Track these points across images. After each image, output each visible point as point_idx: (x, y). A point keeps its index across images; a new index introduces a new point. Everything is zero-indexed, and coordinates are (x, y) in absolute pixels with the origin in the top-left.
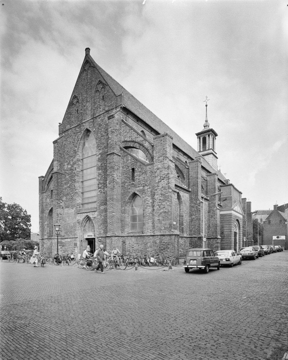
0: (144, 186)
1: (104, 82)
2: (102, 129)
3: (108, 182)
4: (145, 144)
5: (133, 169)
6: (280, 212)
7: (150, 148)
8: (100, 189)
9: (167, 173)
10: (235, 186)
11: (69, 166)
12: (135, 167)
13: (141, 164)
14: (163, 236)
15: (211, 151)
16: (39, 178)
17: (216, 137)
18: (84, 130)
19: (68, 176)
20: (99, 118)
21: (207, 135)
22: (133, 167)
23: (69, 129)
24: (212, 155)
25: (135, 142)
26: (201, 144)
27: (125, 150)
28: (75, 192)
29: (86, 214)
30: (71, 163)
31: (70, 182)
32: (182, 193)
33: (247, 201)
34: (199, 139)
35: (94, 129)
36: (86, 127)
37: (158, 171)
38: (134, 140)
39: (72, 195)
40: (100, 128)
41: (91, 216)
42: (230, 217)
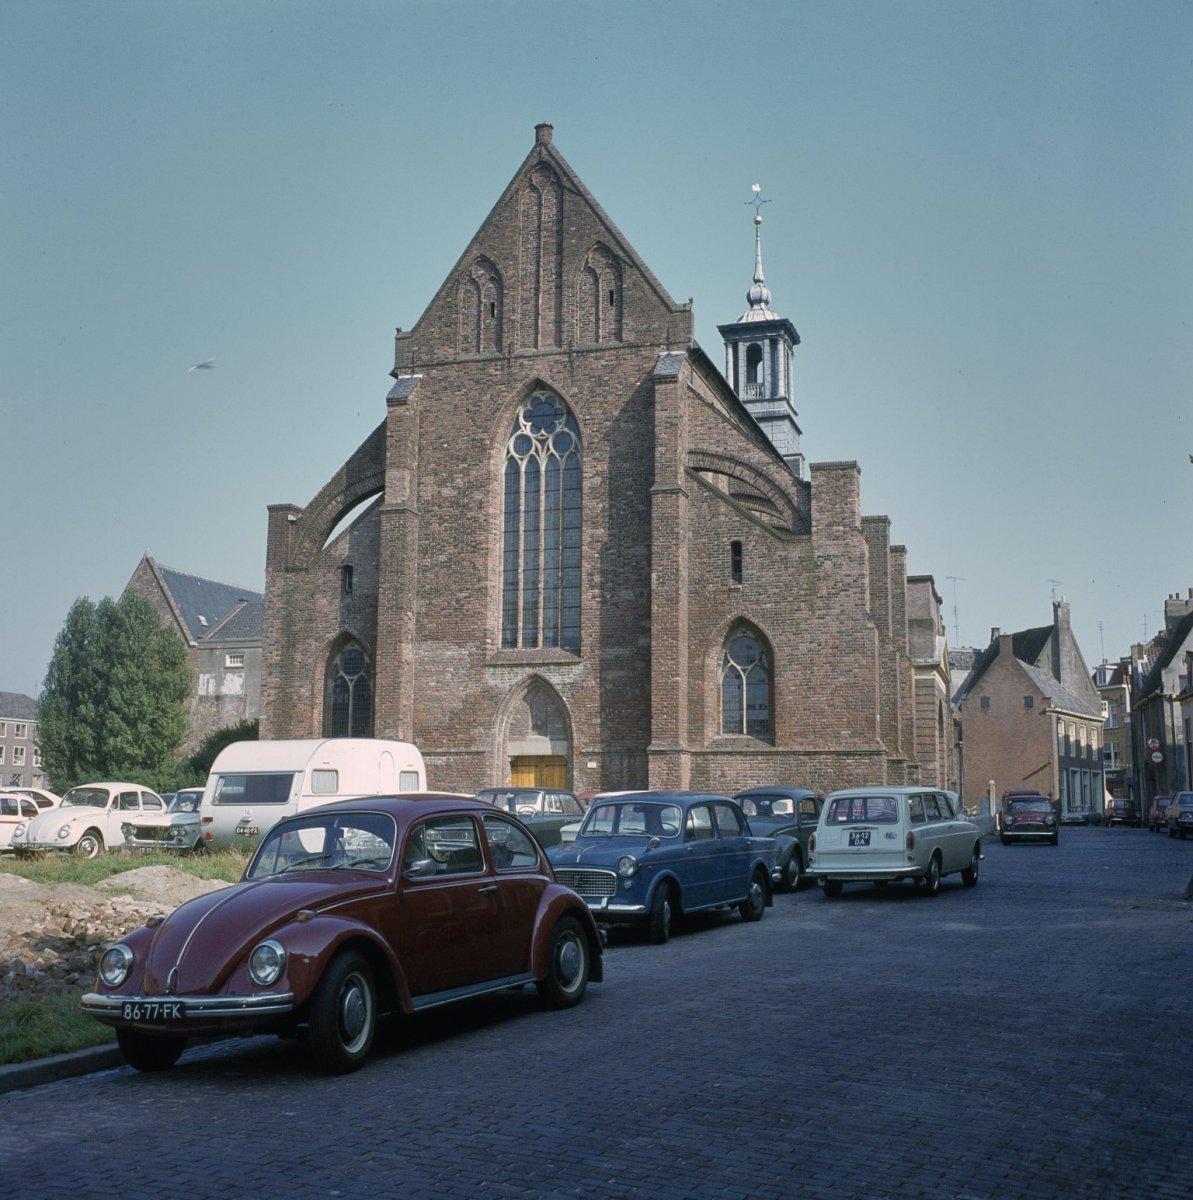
0: (777, 603)
1: (621, 253)
2: (610, 398)
3: (654, 576)
4: (777, 476)
5: (737, 547)
6: (1024, 664)
7: (792, 490)
9: (856, 572)
10: (936, 586)
12: (742, 539)
13: (767, 534)
14: (846, 755)
15: (782, 408)
16: (271, 509)
17: (795, 347)
20: (596, 359)
21: (767, 342)
22: (736, 539)
23: (453, 363)
24: (787, 423)
25: (739, 463)
26: (742, 363)
28: (477, 586)
29: (529, 671)
30: (459, 482)
34: (730, 351)
35: (576, 390)
36: (534, 374)
37: (828, 565)
38: (735, 454)
40: (599, 390)
41: (555, 679)
42: (930, 691)
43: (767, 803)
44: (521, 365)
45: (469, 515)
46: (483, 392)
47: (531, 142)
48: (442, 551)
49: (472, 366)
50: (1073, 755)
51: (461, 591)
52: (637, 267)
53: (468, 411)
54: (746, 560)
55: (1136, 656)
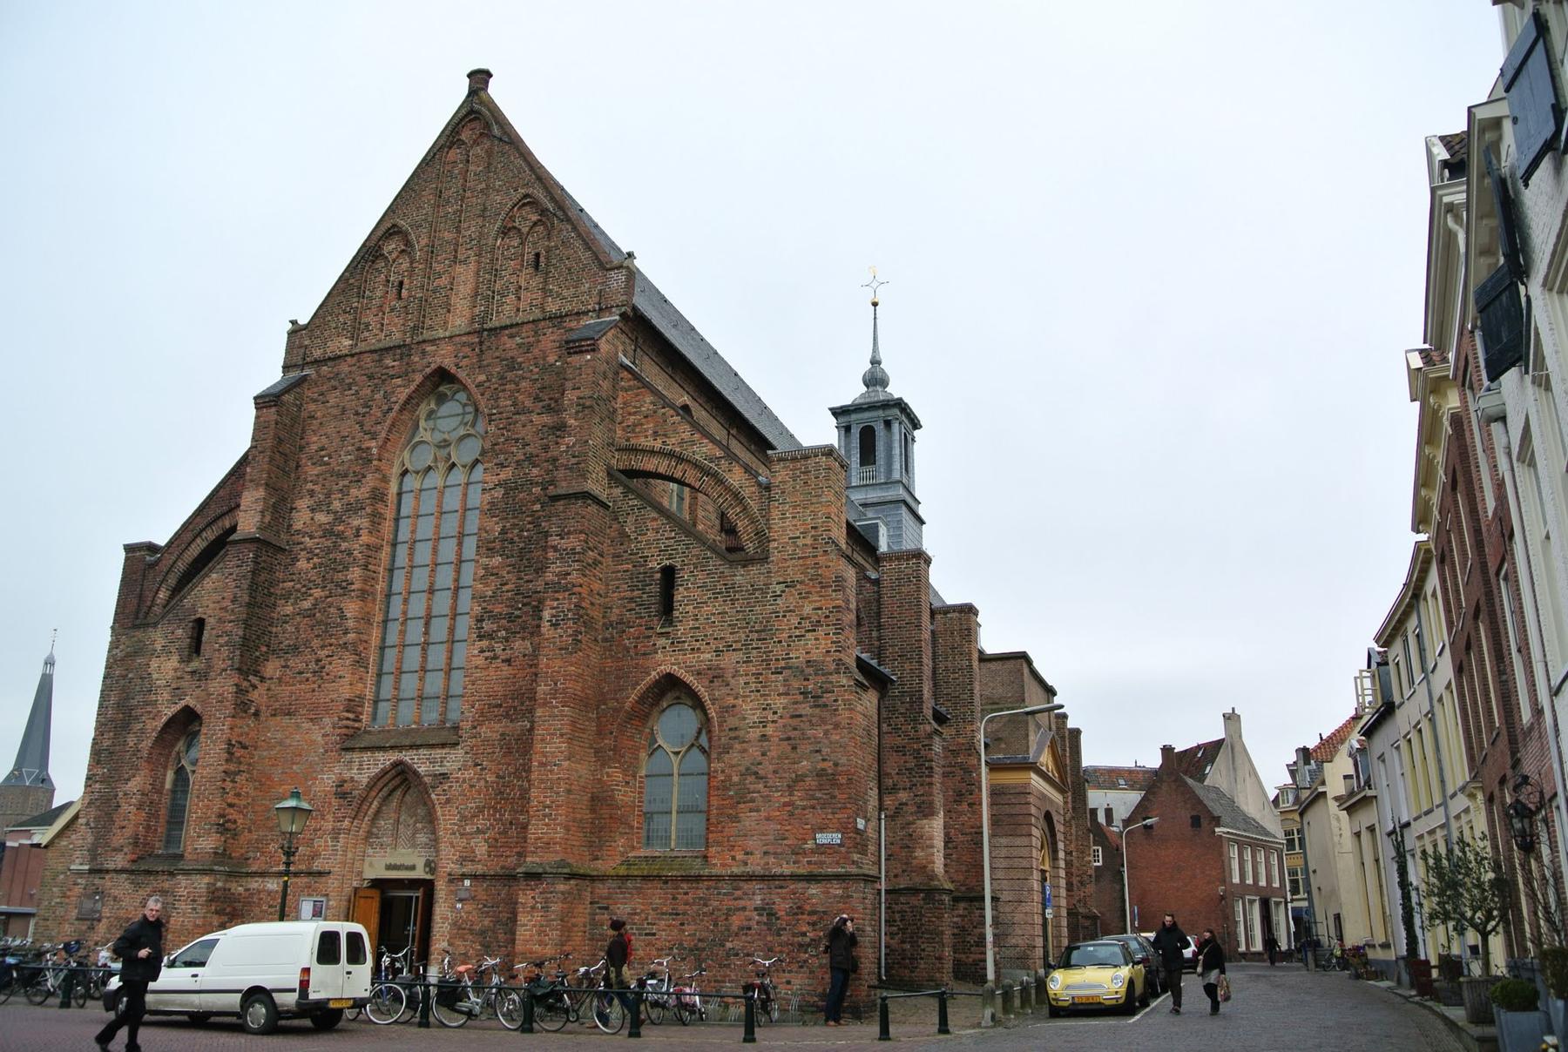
3: (546, 614)
6: (1190, 781)
8: (485, 643)
11: (322, 518)
16: (129, 549)
17: (916, 433)
18: (428, 370)
19: (309, 560)
20: (512, 336)
25: (680, 459)
27: (623, 477)
29: (394, 756)
30: (337, 505)
31: (317, 593)
32: (1453, 813)
33: (1071, 724)
35: (482, 378)
36: (437, 361)
39: (322, 653)
40: (509, 375)
43: (121, 1007)
44: (424, 353)
45: (344, 545)
46: (376, 389)
47: (462, 89)
48: (306, 595)
49: (368, 358)
50: (1250, 881)
51: (323, 647)
52: (569, 220)
53: (357, 414)
54: (680, 594)
55: (1301, 763)
